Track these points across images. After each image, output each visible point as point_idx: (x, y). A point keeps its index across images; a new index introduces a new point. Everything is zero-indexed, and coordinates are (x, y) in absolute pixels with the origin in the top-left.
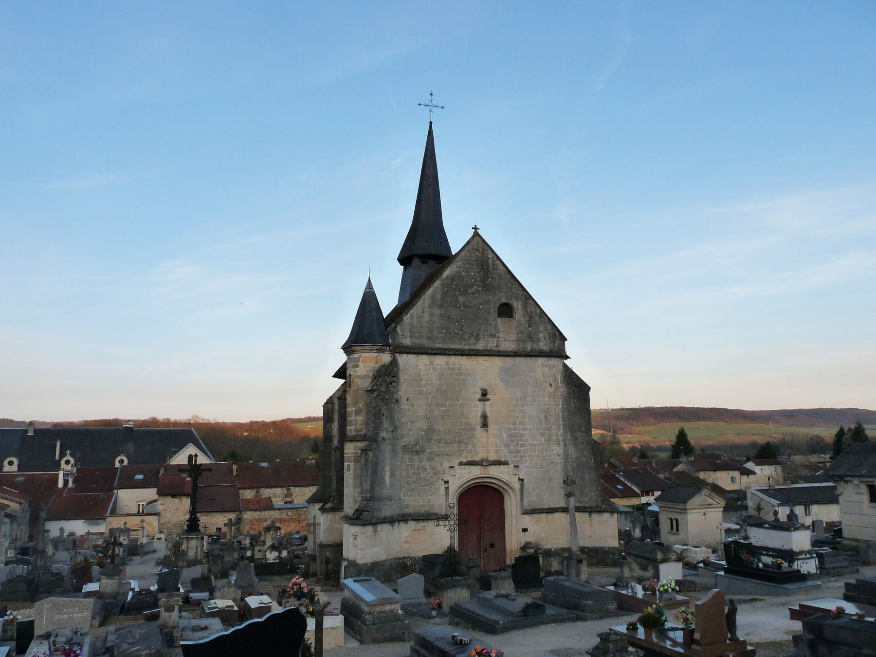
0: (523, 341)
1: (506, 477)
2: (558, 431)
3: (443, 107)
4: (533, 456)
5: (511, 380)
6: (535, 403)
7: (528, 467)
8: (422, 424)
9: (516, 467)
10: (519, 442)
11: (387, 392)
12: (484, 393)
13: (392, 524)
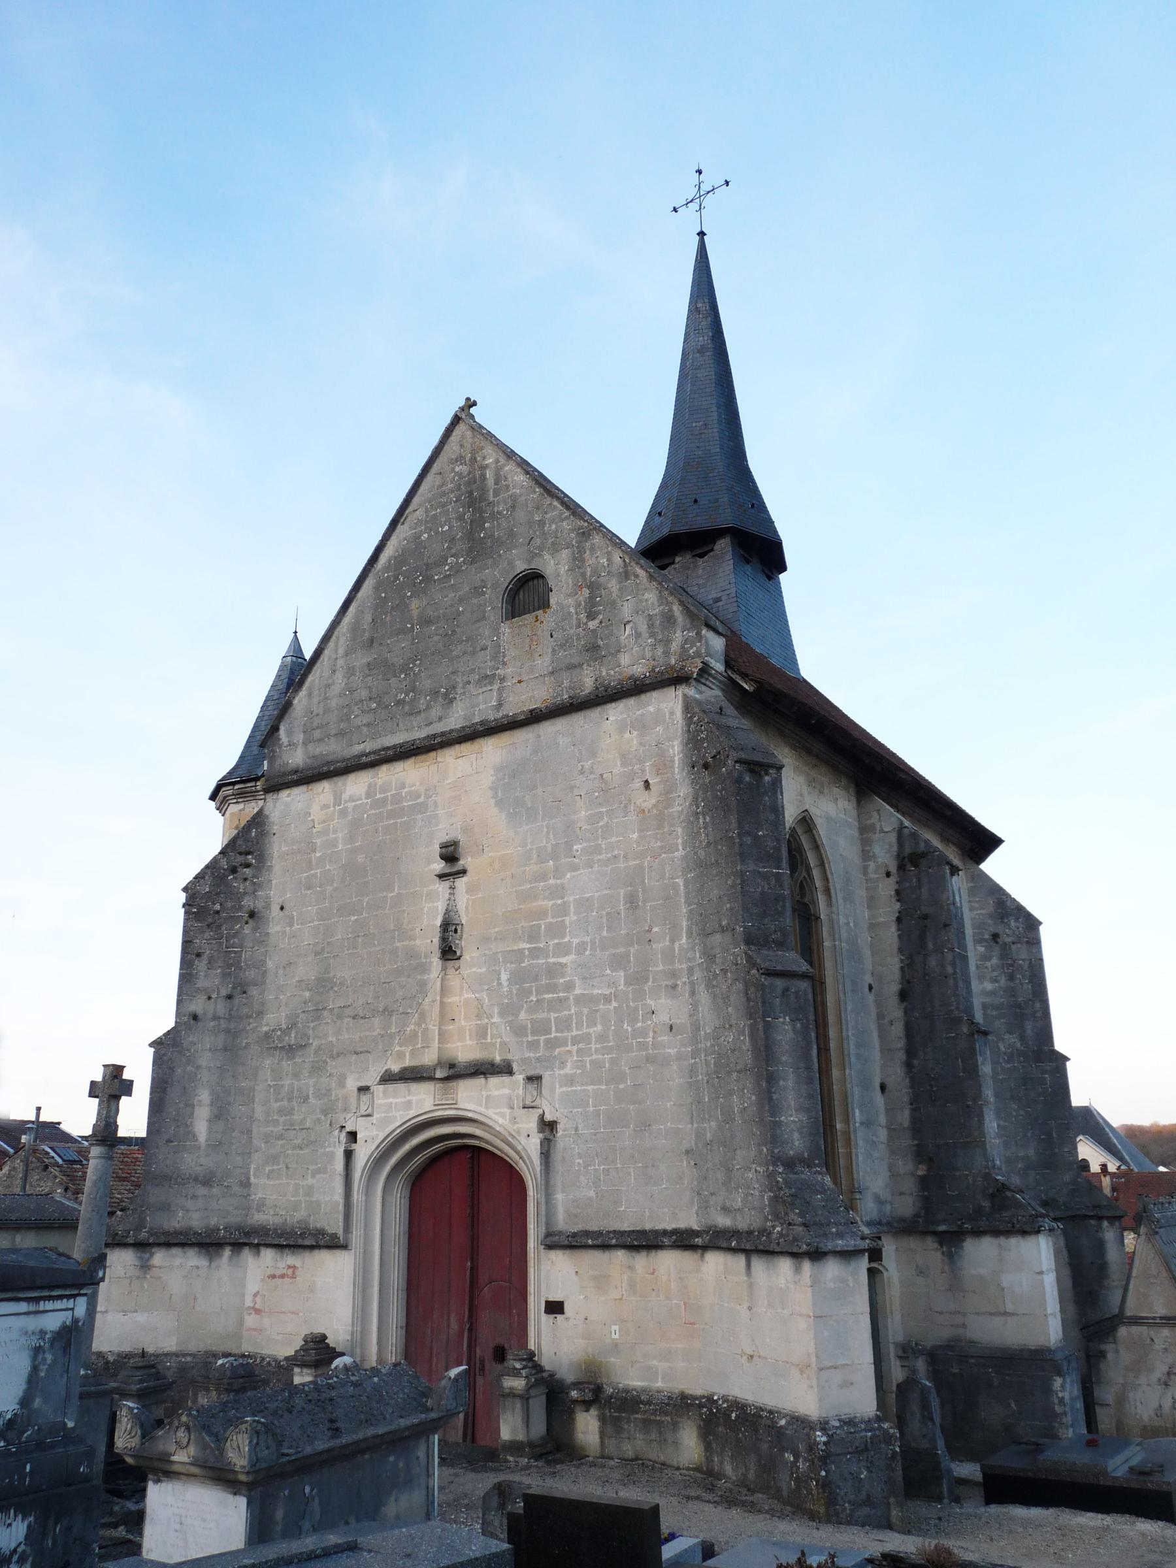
0: (571, 667)
1: (503, 1115)
2: (673, 941)
3: (727, 183)
4: (586, 1038)
5: (527, 799)
6: (597, 857)
7: (570, 1081)
8: (305, 970)
9: (534, 1079)
10: (546, 996)
11: (218, 894)
12: (450, 854)
13: (208, 1253)
